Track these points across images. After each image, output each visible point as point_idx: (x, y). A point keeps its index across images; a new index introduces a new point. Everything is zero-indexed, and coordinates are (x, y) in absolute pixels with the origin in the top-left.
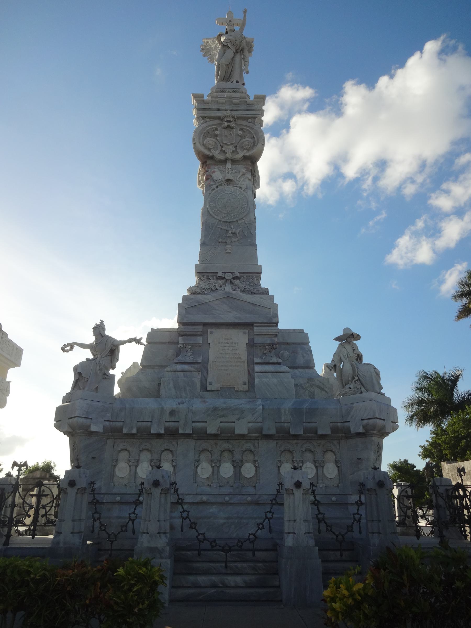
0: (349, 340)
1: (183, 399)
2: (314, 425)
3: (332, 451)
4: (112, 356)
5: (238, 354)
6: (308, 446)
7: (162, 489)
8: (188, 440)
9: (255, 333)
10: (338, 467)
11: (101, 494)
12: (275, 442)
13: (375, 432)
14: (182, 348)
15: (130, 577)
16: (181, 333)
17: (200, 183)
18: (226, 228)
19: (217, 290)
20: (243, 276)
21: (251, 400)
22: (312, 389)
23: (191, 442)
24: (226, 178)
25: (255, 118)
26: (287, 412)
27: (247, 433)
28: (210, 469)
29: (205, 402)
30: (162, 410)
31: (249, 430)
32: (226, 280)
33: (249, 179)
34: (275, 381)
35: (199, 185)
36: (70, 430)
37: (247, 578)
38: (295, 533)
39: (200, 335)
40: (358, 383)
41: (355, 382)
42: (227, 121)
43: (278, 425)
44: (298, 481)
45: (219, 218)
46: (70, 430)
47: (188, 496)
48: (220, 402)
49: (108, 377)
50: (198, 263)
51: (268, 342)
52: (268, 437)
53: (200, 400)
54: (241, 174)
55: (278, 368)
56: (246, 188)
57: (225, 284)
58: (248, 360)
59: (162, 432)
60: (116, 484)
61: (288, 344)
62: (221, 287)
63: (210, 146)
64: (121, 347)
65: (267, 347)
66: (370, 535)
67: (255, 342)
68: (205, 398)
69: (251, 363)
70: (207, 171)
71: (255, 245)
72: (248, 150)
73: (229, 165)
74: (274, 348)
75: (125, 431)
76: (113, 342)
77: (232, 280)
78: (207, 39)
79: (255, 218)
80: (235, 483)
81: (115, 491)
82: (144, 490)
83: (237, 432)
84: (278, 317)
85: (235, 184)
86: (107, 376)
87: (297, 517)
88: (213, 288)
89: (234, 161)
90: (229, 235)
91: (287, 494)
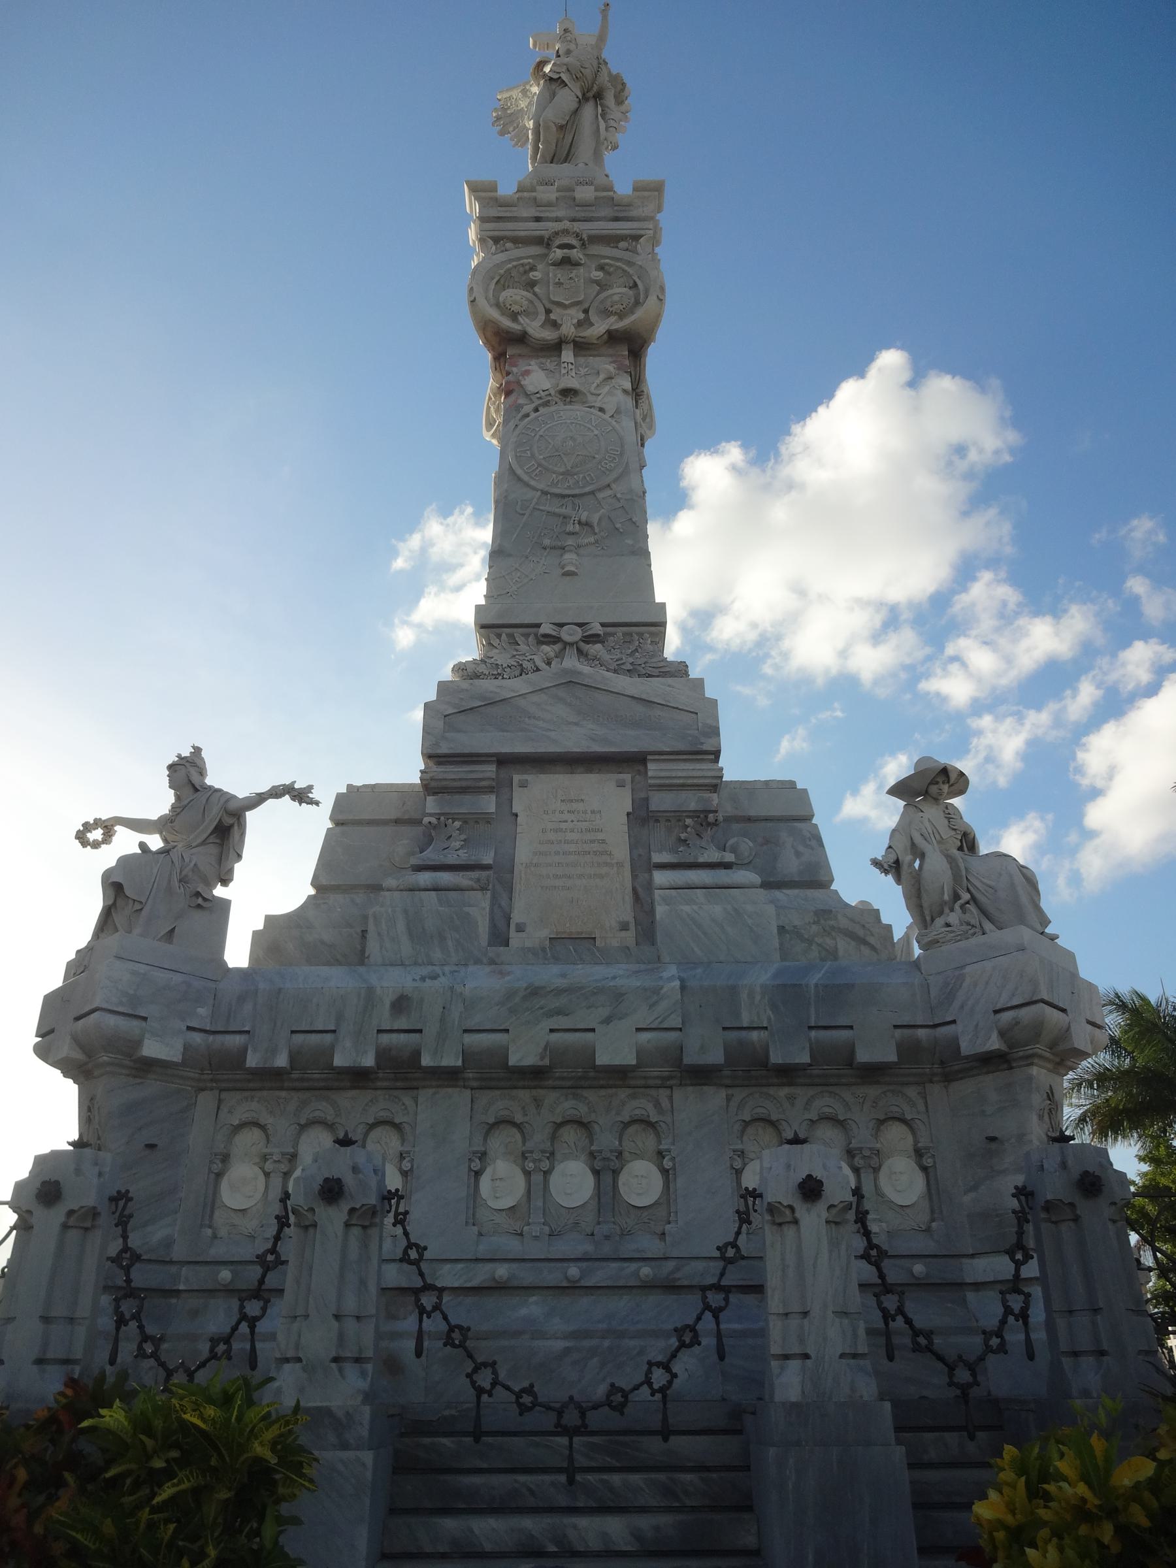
0: (934, 789)
1: (437, 969)
2: (845, 1034)
3: (903, 1120)
4: (222, 845)
5: (603, 842)
6: (825, 1103)
7: (352, 1211)
8: (450, 1090)
9: (651, 781)
10: (924, 1169)
11: (171, 1262)
12: (723, 1093)
13: (1040, 1048)
14: (435, 827)
15: (149, 1443)
16: (433, 784)
17: (490, 425)
18: (563, 511)
19: (538, 670)
20: (613, 634)
21: (643, 967)
22: (828, 941)
23: (460, 1098)
24: (562, 386)
25: (636, 238)
26: (758, 998)
27: (634, 1062)
28: (520, 1181)
29: (502, 974)
30: (370, 997)
31: (639, 1053)
32: (566, 644)
33: (625, 391)
34: (717, 910)
35: (488, 430)
36: (78, 1055)
37: (645, 1522)
38: (806, 1356)
39: (490, 790)
40: (971, 907)
41: (962, 907)
42: (561, 247)
43: (733, 1035)
44: (809, 1176)
45: (541, 486)
46: (78, 1055)
47: (448, 1266)
48: (549, 974)
49: (205, 904)
50: (483, 602)
51: (693, 806)
52: (701, 1075)
53: (488, 969)
54: (602, 376)
55: (723, 876)
56: (618, 411)
57: (560, 655)
58: (632, 860)
59: (369, 1061)
60: (223, 1232)
61: (749, 819)
62: (549, 664)
63: (515, 308)
64: (250, 816)
65: (688, 821)
66: (1067, 1362)
67: (653, 807)
68: (502, 964)
69: (642, 866)
70: (508, 374)
71: (647, 554)
72: (621, 315)
73: (567, 355)
74: (709, 824)
75: (252, 1061)
76: (227, 801)
77: (582, 644)
78: (507, 90)
79: (644, 493)
80: (599, 1223)
81: (217, 1251)
82: (292, 1219)
83: (602, 1059)
84: (718, 735)
85: (584, 403)
86: (205, 899)
87: (812, 1289)
88: (526, 664)
89: (581, 347)
90: (570, 528)
91: (774, 1223)
